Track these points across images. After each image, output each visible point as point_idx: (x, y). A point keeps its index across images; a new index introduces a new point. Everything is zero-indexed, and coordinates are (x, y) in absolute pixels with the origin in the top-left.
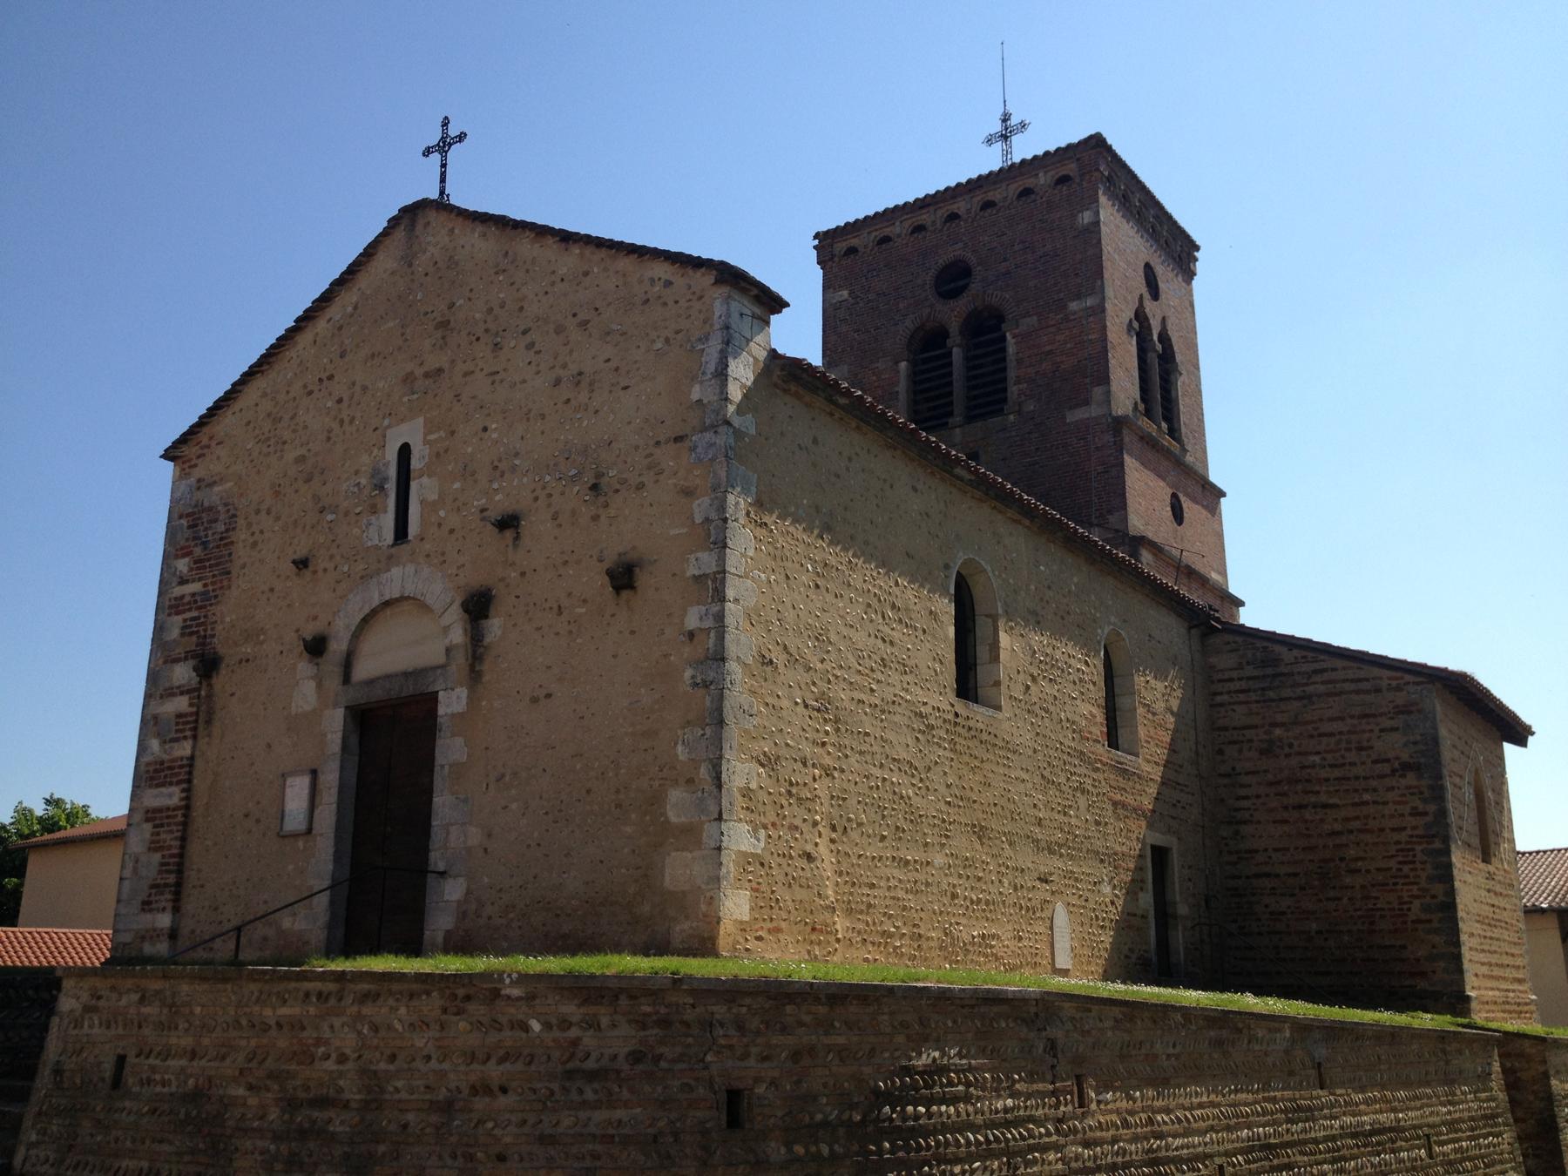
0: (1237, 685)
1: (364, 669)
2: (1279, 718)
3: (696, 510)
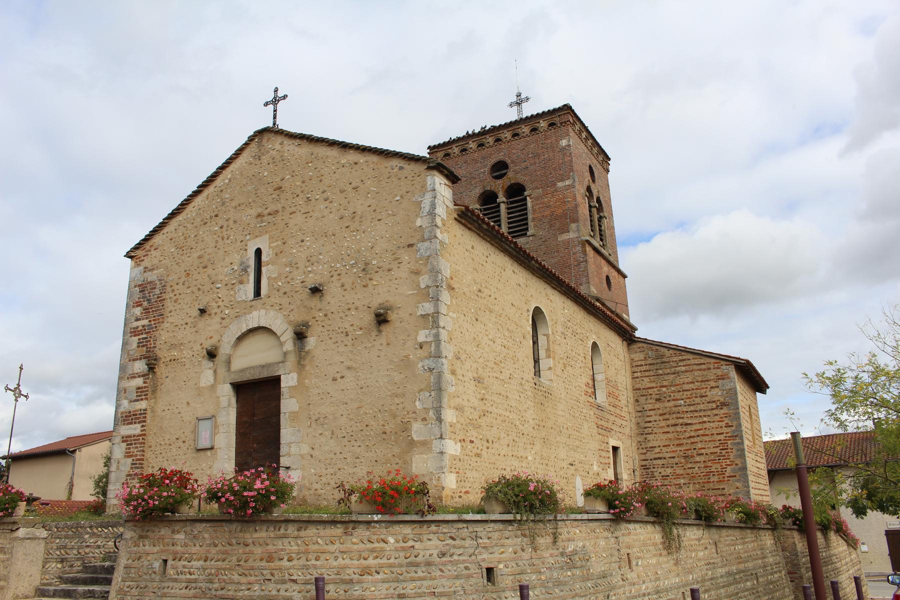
0: (644, 368)
1: (237, 365)
2: (665, 383)
3: (421, 282)
